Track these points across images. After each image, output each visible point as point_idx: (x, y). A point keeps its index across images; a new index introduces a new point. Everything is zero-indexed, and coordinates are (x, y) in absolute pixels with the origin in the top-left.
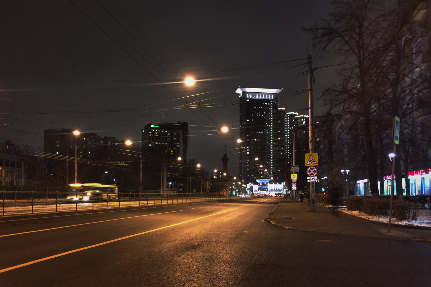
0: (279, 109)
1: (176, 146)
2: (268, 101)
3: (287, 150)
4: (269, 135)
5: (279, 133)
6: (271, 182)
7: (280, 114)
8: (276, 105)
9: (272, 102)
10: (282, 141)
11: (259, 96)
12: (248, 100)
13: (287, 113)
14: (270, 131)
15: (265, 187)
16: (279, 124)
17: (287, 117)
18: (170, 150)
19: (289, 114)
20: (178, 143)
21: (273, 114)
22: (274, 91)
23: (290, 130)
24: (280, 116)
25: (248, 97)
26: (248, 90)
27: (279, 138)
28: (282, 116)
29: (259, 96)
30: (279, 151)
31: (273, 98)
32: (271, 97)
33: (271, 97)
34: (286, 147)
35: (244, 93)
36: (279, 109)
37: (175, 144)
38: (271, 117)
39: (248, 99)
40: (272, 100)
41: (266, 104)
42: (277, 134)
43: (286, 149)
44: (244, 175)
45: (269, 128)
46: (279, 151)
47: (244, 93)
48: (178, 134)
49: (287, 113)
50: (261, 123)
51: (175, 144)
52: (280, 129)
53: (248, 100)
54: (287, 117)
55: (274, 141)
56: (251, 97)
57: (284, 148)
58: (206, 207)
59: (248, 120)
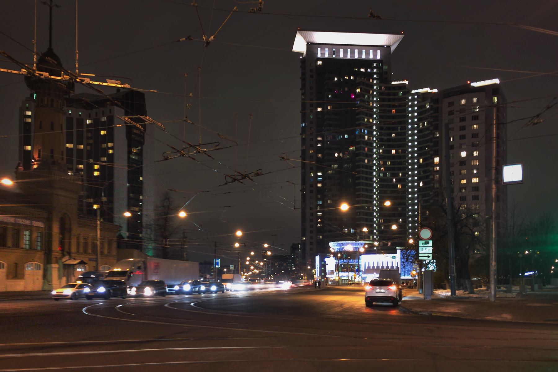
0: (393, 83)
1: (104, 152)
2: (367, 63)
3: (413, 121)
4: (369, 144)
5: (394, 139)
6: (370, 251)
7: (397, 94)
8: (386, 73)
9: (377, 67)
10: (400, 157)
11: (345, 52)
12: (320, 63)
13: (413, 92)
14: (370, 133)
15: (353, 262)
16: (394, 117)
17: (413, 100)
18: (92, 165)
19: (417, 94)
20: (110, 145)
21: (380, 94)
22: (382, 39)
23: (420, 131)
24: (393, 99)
25: (319, 55)
26: (319, 37)
27: (393, 152)
28: (400, 99)
29: (345, 52)
30: (393, 169)
31: (379, 57)
32: (375, 55)
33: (375, 55)
34: (409, 170)
35: (311, 46)
36: (393, 83)
37: (104, 146)
38: (373, 102)
39: (319, 59)
40: (377, 61)
41: (362, 70)
42: (389, 140)
43: (409, 176)
44: (311, 238)
45: (371, 126)
46: (393, 169)
47: (311, 46)
48: (111, 120)
49: (413, 92)
50: (349, 116)
51: (104, 146)
52: (394, 130)
53: (320, 63)
54: (413, 100)
55: (381, 157)
56: (327, 55)
57: (405, 174)
58: (457, 311)
59: (320, 109)
